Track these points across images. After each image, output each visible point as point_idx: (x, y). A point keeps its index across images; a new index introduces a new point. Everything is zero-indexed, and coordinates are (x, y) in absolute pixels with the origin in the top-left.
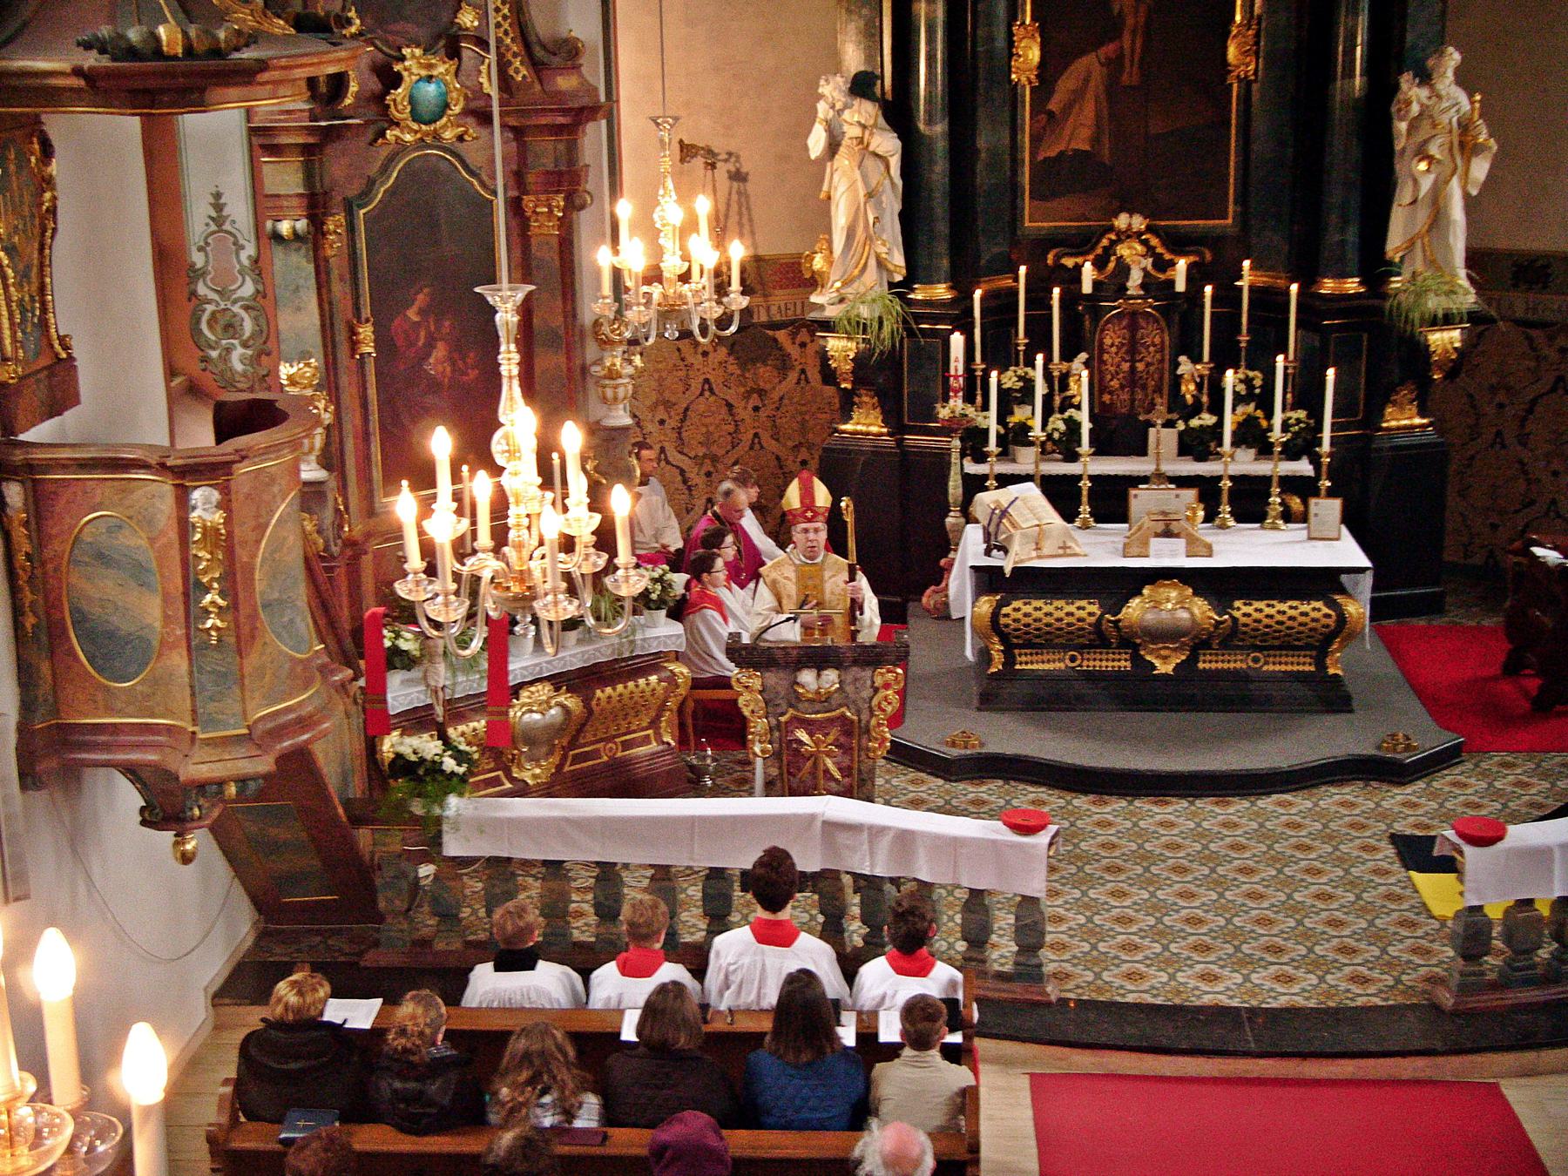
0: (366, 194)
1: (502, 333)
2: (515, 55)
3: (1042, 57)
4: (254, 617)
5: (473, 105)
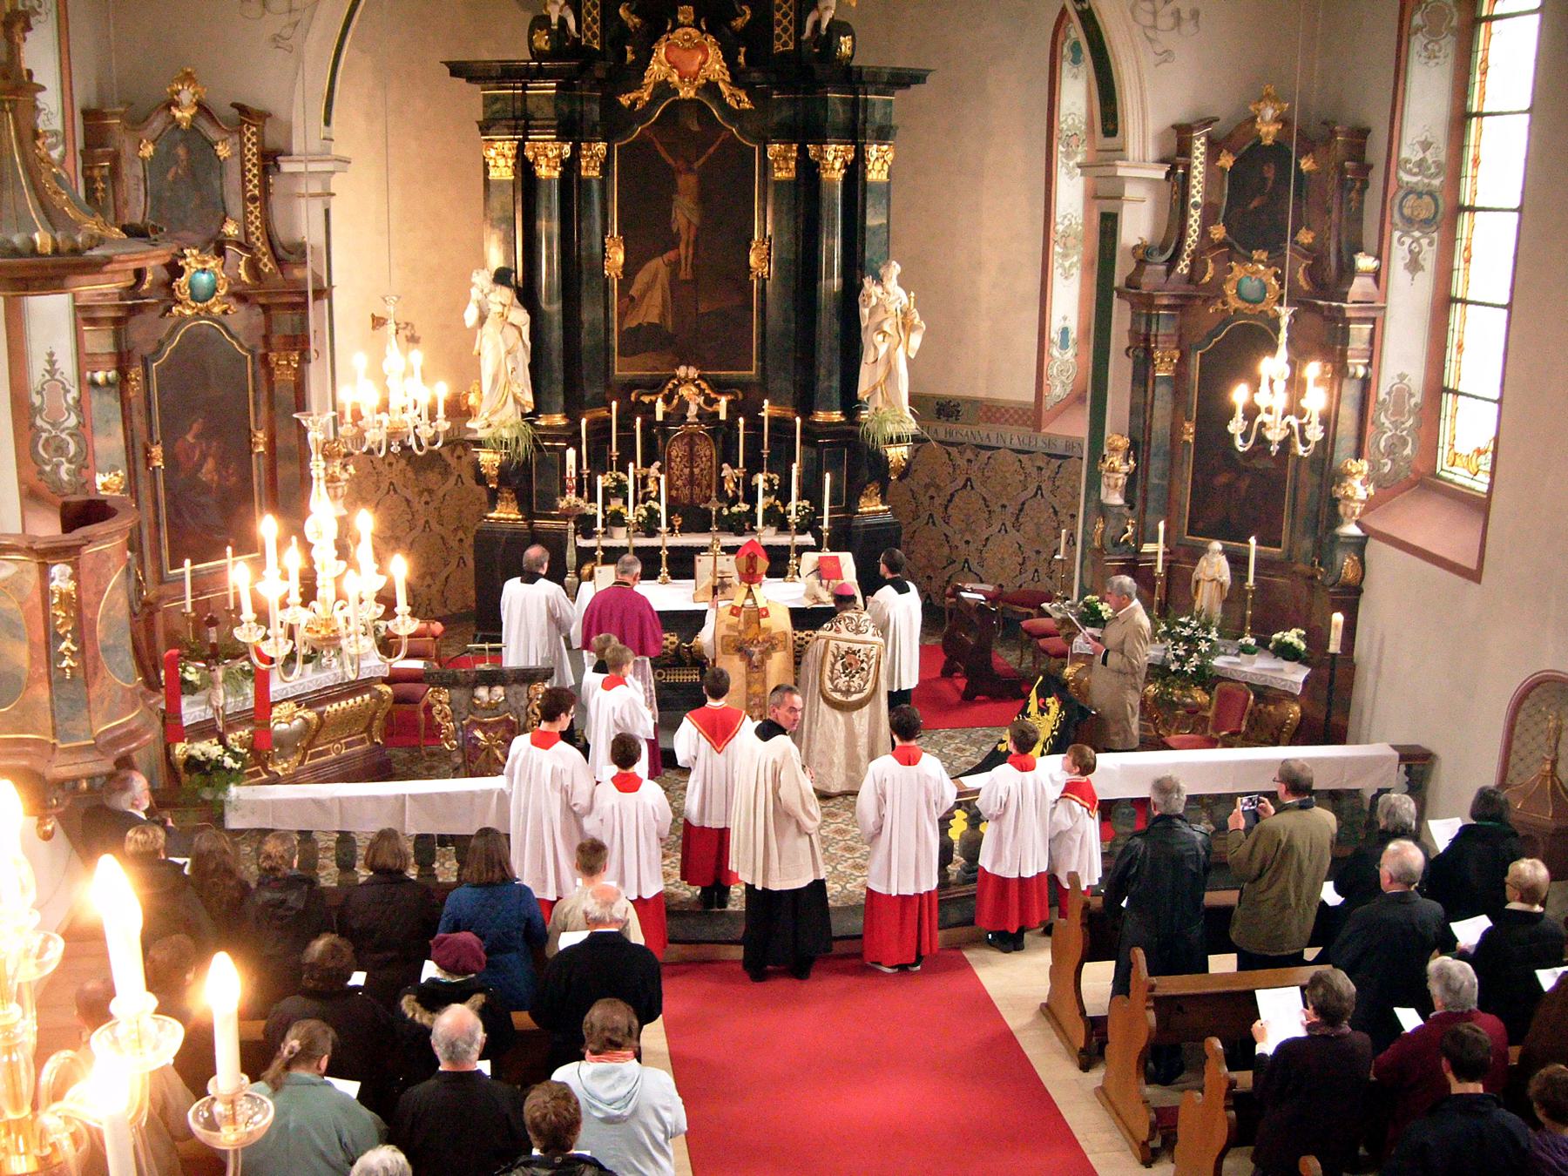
0: (157, 352)
1: (313, 447)
2: (264, 254)
4: (96, 657)
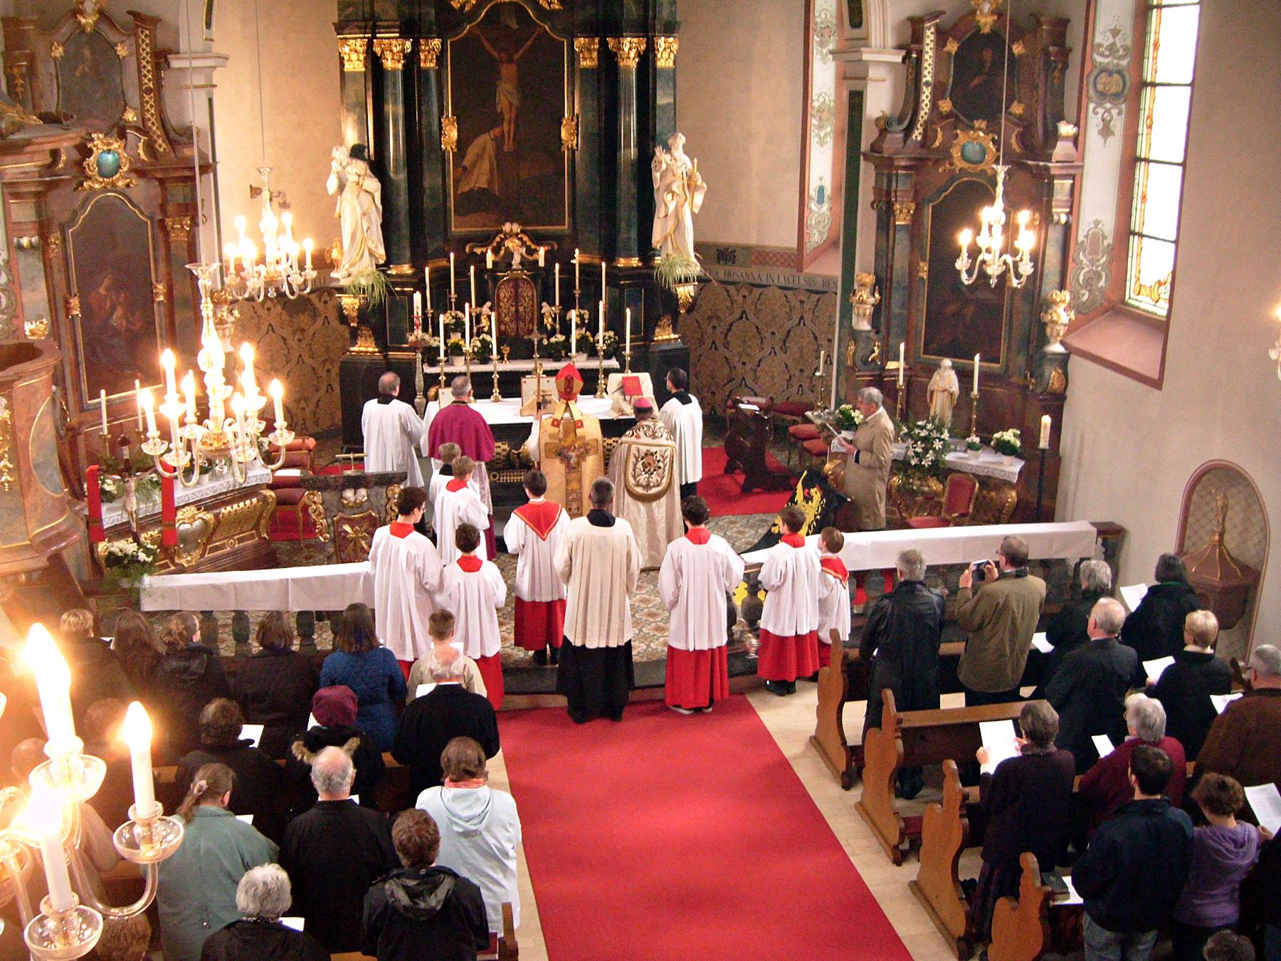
0: (73, 220)
2: (158, 137)
3: (459, 135)
5: (135, 166)
